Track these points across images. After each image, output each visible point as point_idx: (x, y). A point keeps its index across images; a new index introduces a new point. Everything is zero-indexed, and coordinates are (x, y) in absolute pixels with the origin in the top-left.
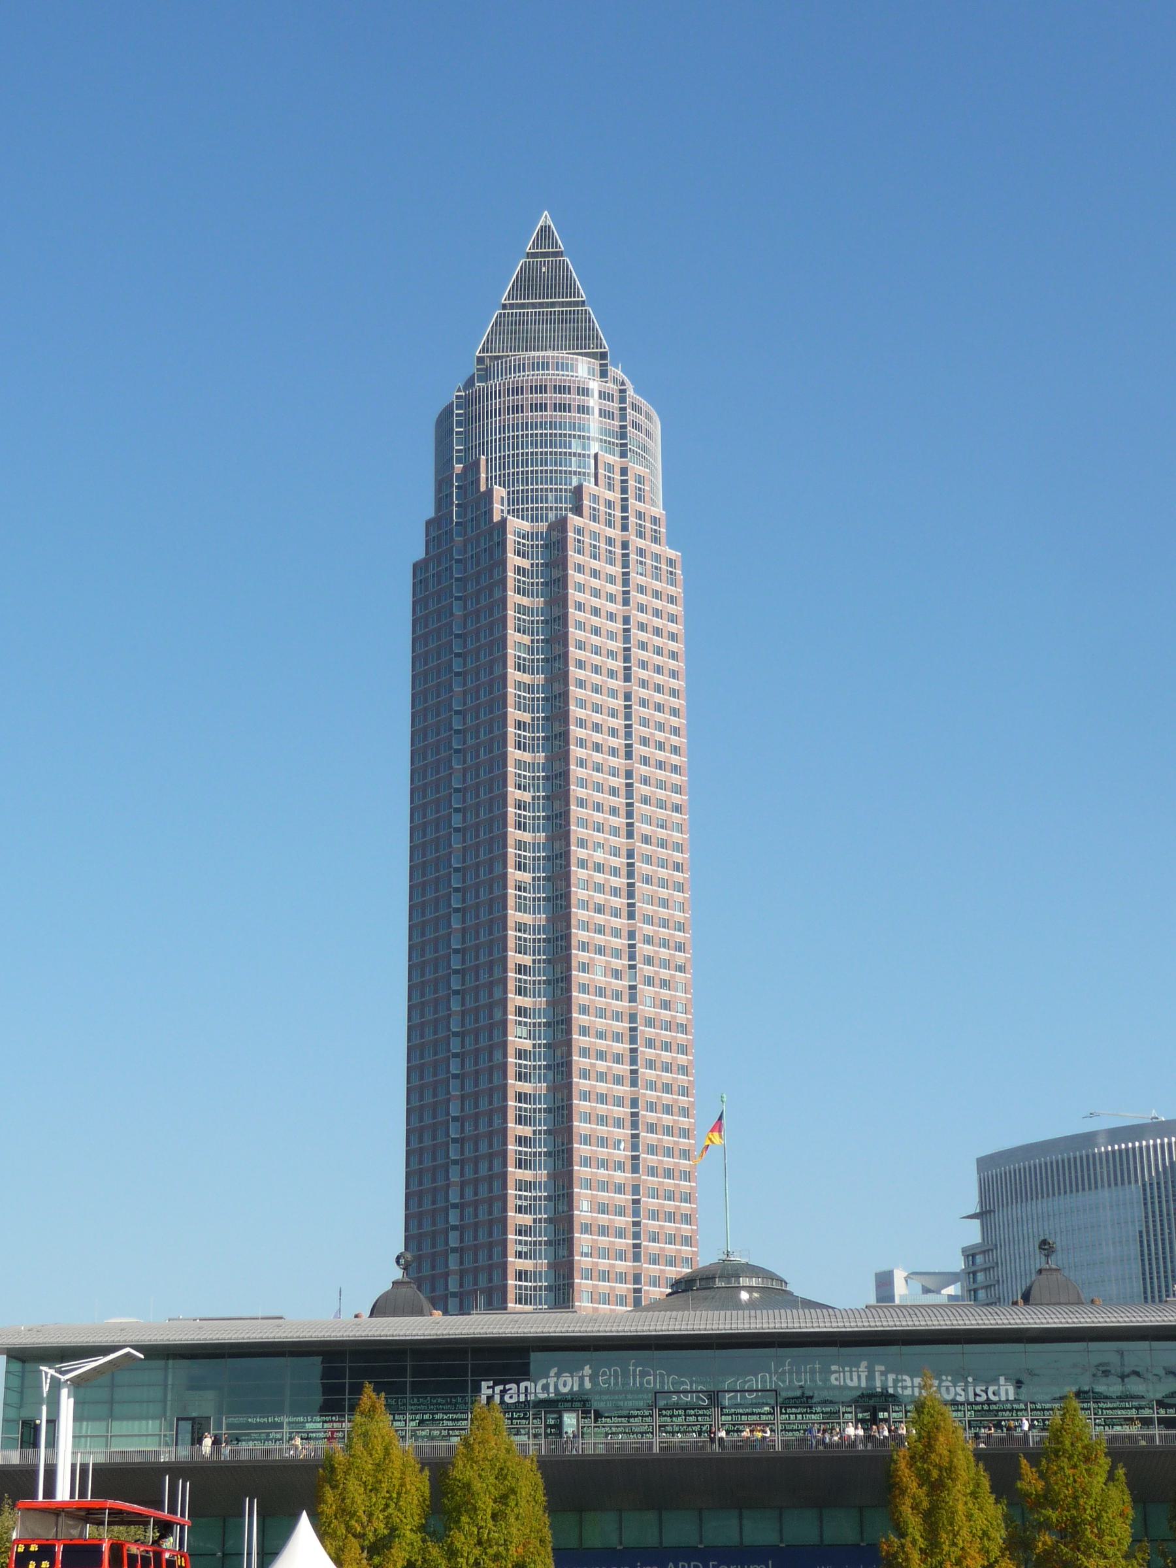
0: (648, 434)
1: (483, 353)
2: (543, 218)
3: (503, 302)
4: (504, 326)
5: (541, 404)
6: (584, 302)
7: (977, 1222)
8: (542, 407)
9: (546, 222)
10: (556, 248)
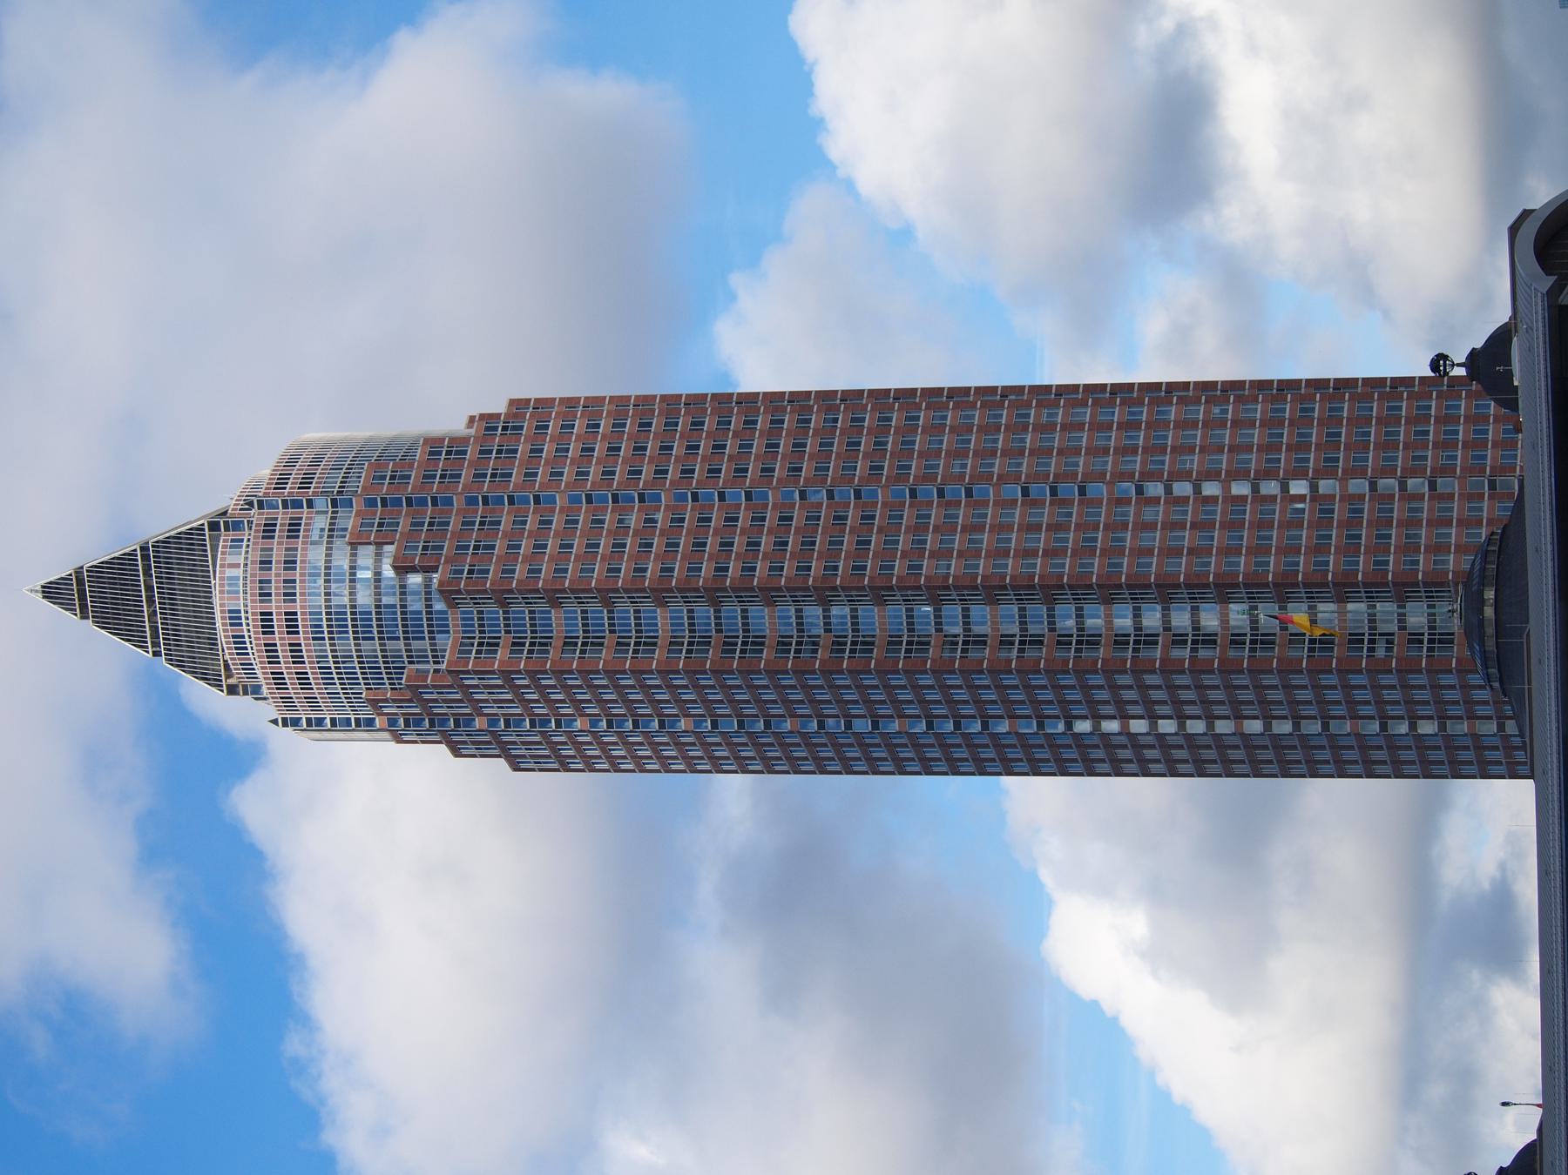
4: (183, 656)
5: (287, 620)
7: (1541, 1110)
10: (72, 580)
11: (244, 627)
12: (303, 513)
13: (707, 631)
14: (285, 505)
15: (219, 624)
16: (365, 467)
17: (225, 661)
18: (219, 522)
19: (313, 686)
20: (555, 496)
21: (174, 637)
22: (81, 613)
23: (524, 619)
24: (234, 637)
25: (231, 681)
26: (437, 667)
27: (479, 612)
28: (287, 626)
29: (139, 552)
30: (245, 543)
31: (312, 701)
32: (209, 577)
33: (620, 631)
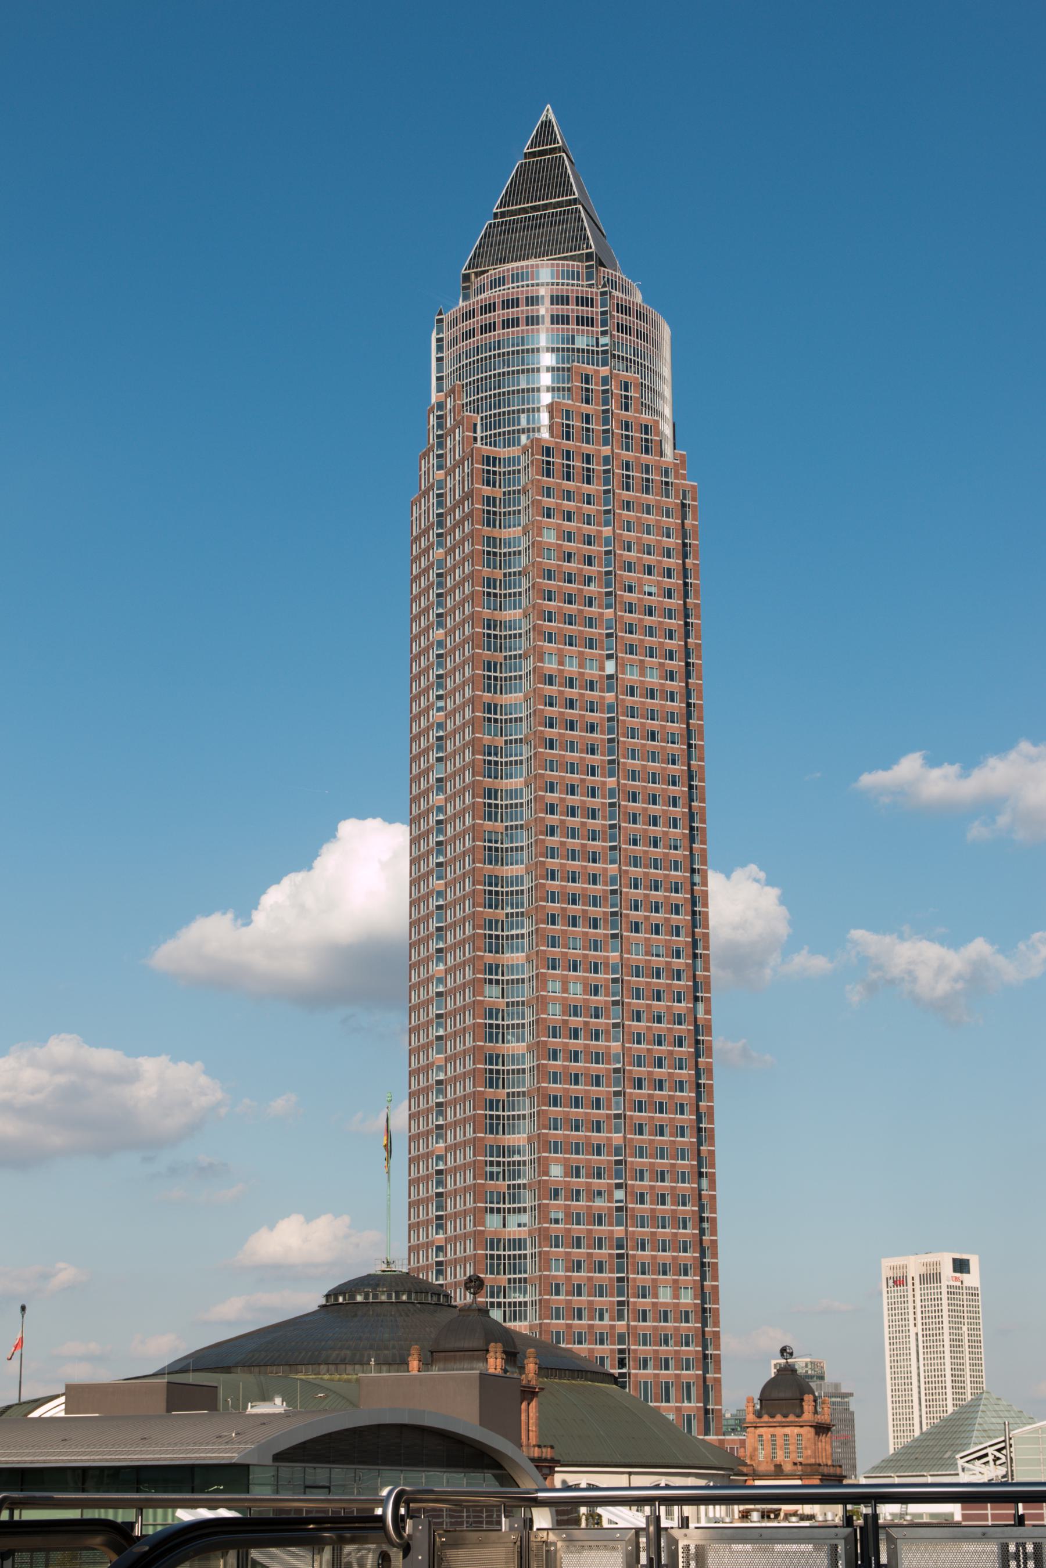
0: (641, 335)
2: (545, 112)
3: (495, 211)
6: (575, 199)
9: (547, 116)
11: (511, 286)
12: (597, 327)
13: (506, 648)
14: (603, 313)
15: (514, 265)
16: (636, 375)
17: (488, 271)
18: (593, 260)
19: (465, 342)
21: (508, 229)
22: (529, 153)
23: (514, 506)
24: (504, 277)
25: (473, 275)
26: (479, 439)
27: (519, 511)
28: (508, 320)
31: (454, 342)
32: (547, 256)
33: (505, 581)
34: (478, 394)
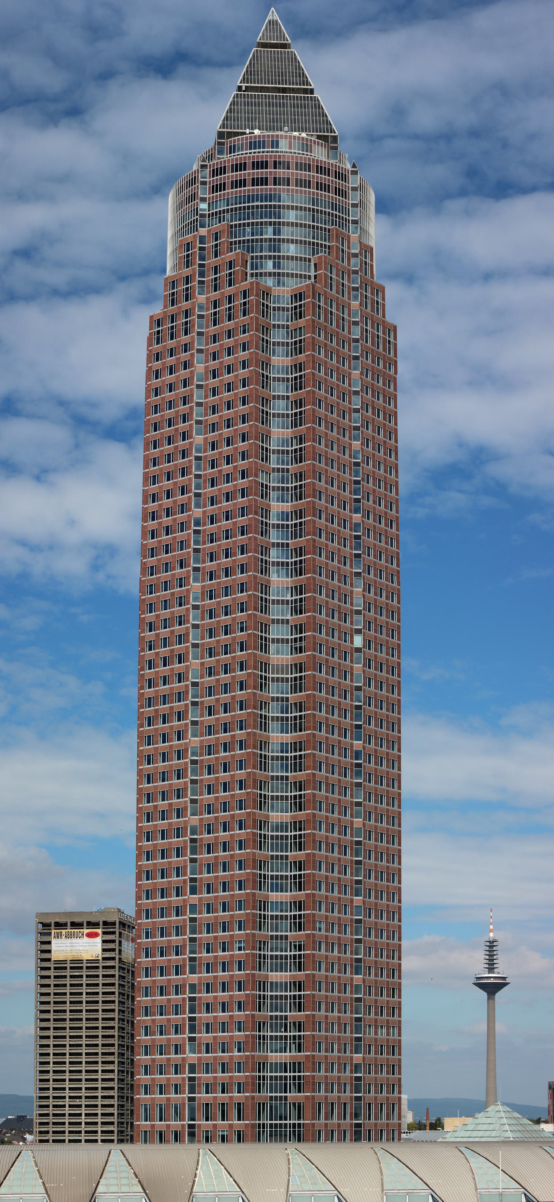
1: (224, 128)
2: (270, 13)
8: (264, 181)
11: (249, 151)
20: (359, 441)
29: (309, 87)
30: (305, 153)
34: (216, 208)
